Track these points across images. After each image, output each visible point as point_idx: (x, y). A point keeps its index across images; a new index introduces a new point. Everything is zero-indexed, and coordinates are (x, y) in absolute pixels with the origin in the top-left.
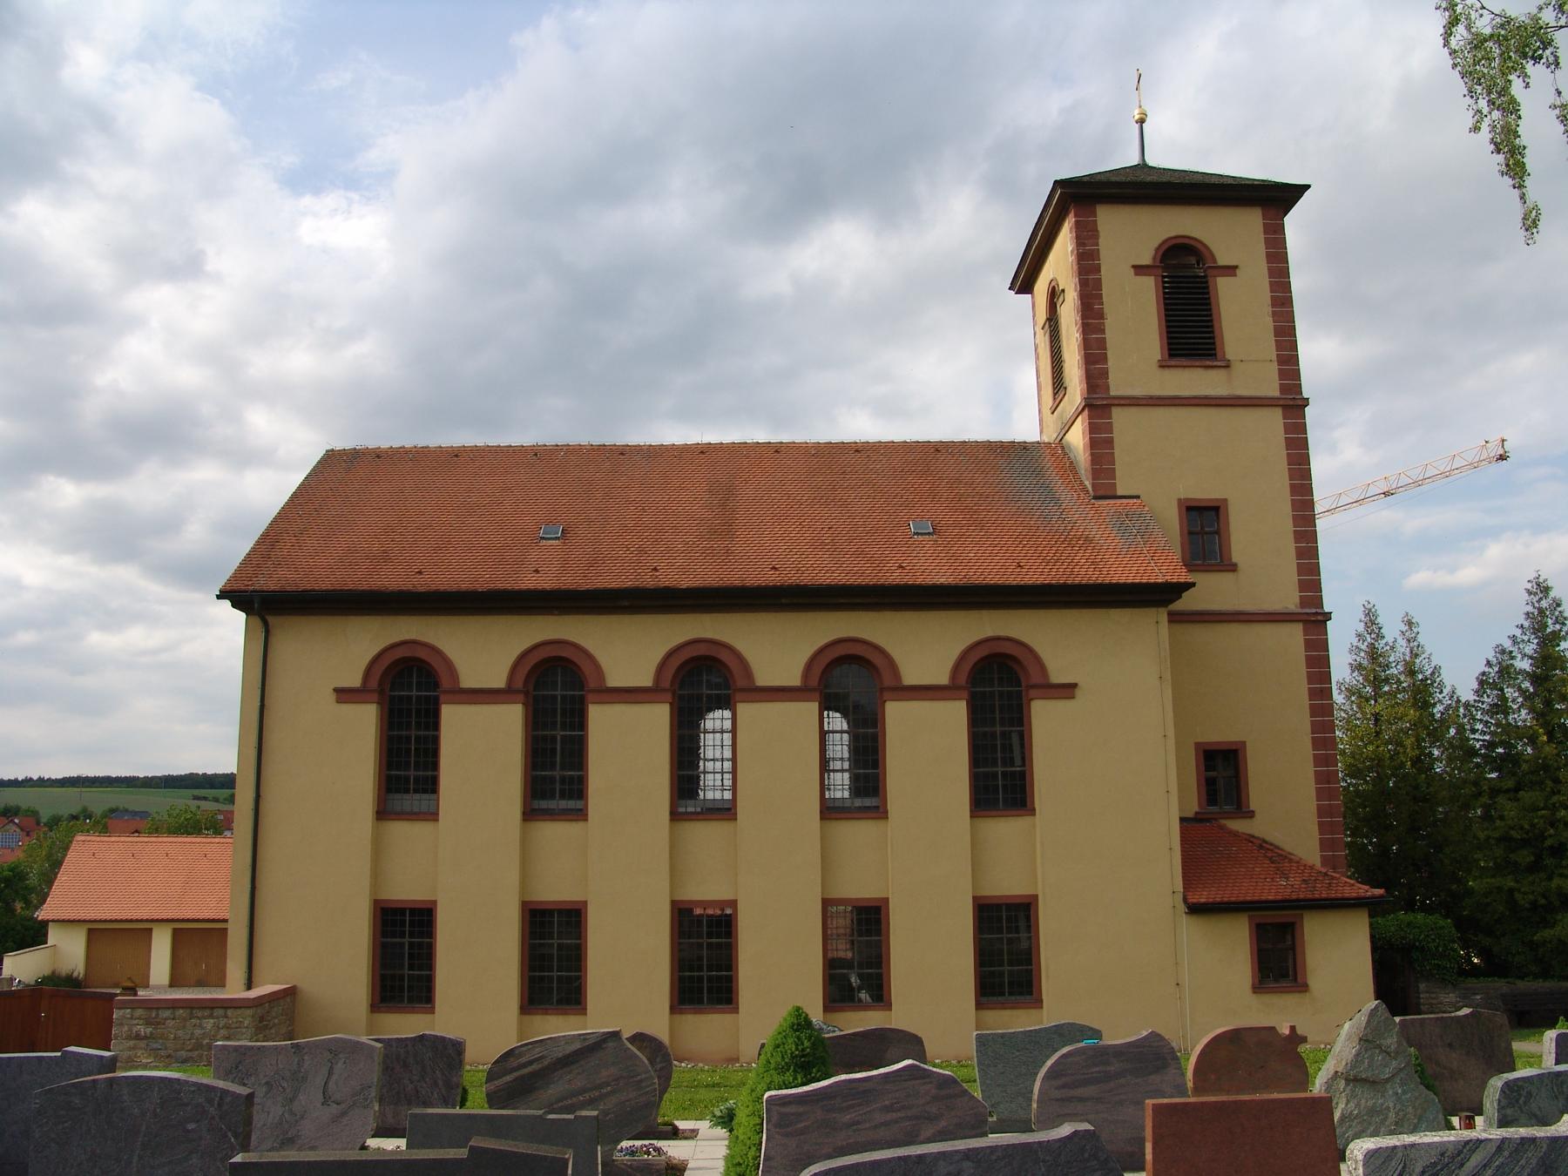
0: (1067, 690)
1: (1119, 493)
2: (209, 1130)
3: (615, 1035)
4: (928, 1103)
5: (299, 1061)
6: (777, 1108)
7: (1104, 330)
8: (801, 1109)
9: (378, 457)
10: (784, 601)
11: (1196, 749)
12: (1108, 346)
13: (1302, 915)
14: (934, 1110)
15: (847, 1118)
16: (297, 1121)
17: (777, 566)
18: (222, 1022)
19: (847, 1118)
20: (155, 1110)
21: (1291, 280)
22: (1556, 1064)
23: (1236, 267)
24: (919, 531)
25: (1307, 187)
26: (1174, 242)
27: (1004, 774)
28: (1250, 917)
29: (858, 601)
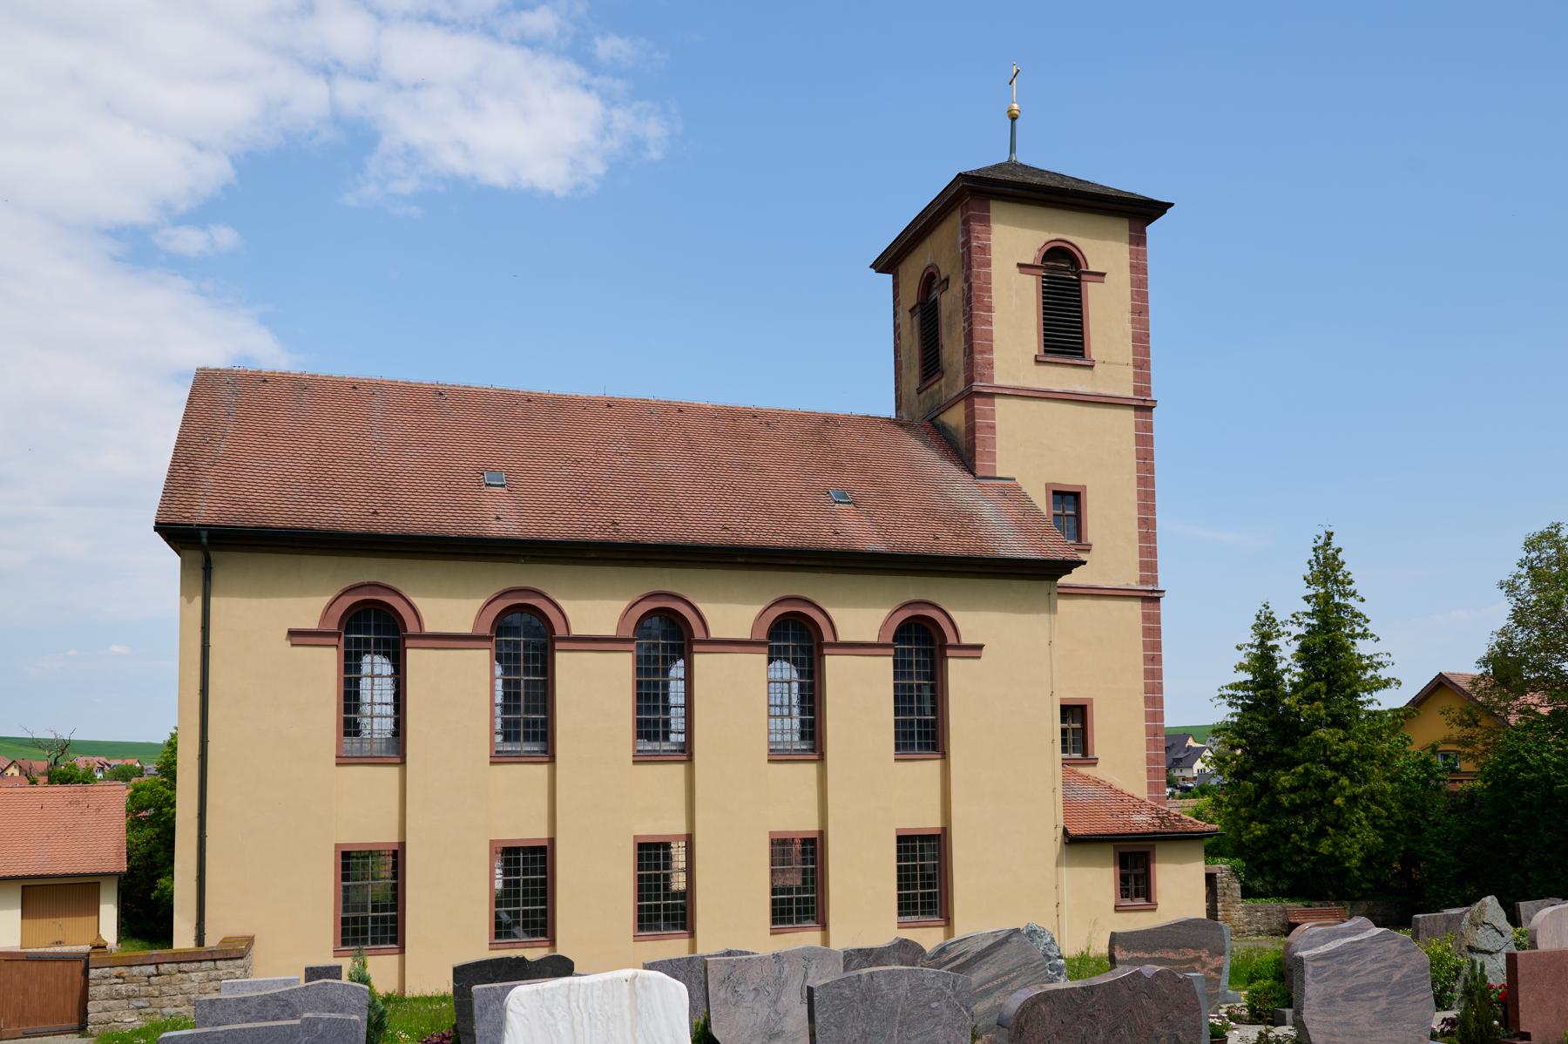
1: (998, 475)
2: (947, 1007)
3: (1017, 931)
4: (1397, 956)
5: (780, 968)
6: (1311, 963)
7: (991, 322)
8: (1324, 963)
9: (609, 406)
10: (739, 560)
12: (994, 338)
13: (1154, 845)
14: (1399, 960)
15: (1352, 968)
16: (781, 1019)
17: (379, 511)
19: (1352, 968)
20: (907, 994)
21: (1149, 290)
24: (491, 483)
25: (1172, 205)
27: (919, 721)
28: (1114, 846)
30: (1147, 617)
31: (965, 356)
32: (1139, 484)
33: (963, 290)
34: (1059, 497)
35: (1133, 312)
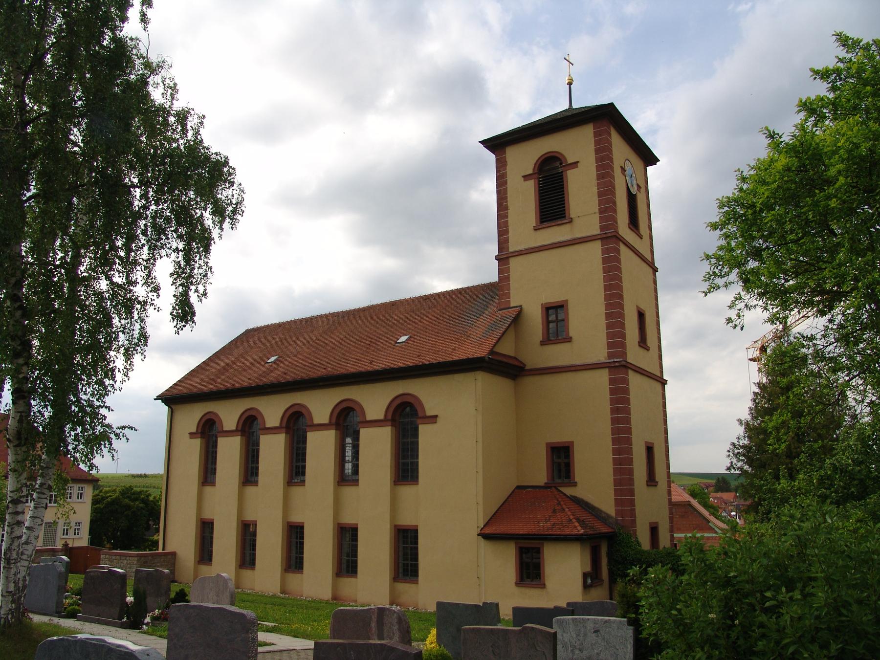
0: (434, 419)
1: (511, 306)
10: (321, 384)
11: (547, 447)
18: (129, 561)
22: (556, 632)
23: (578, 162)
26: (543, 157)
28: (515, 543)
29: (341, 382)
35: (598, 179)
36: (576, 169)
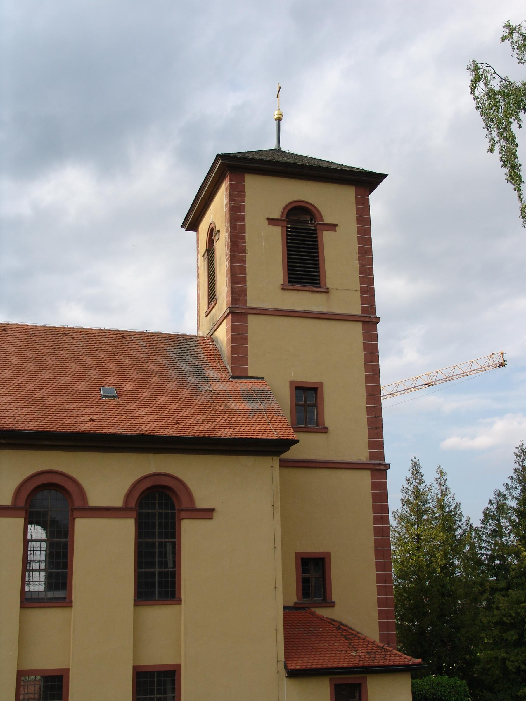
7: (245, 261)
13: (366, 677)
24: (107, 395)
25: (386, 176)
28: (330, 679)
30: (374, 486)
31: (226, 286)
32: (367, 381)
33: (226, 238)
34: (301, 392)
36: (334, 232)
